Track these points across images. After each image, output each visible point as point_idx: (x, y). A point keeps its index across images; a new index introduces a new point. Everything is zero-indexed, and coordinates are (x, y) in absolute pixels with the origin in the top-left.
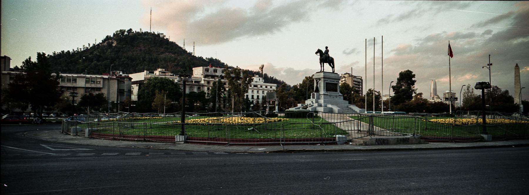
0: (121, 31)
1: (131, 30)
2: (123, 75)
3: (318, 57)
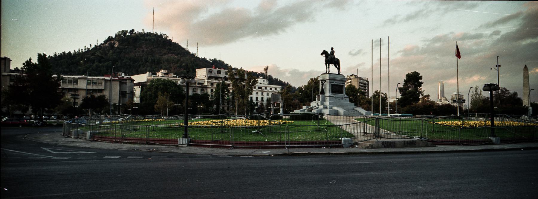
0: (123, 31)
1: (133, 30)
2: (125, 77)
3: (323, 58)
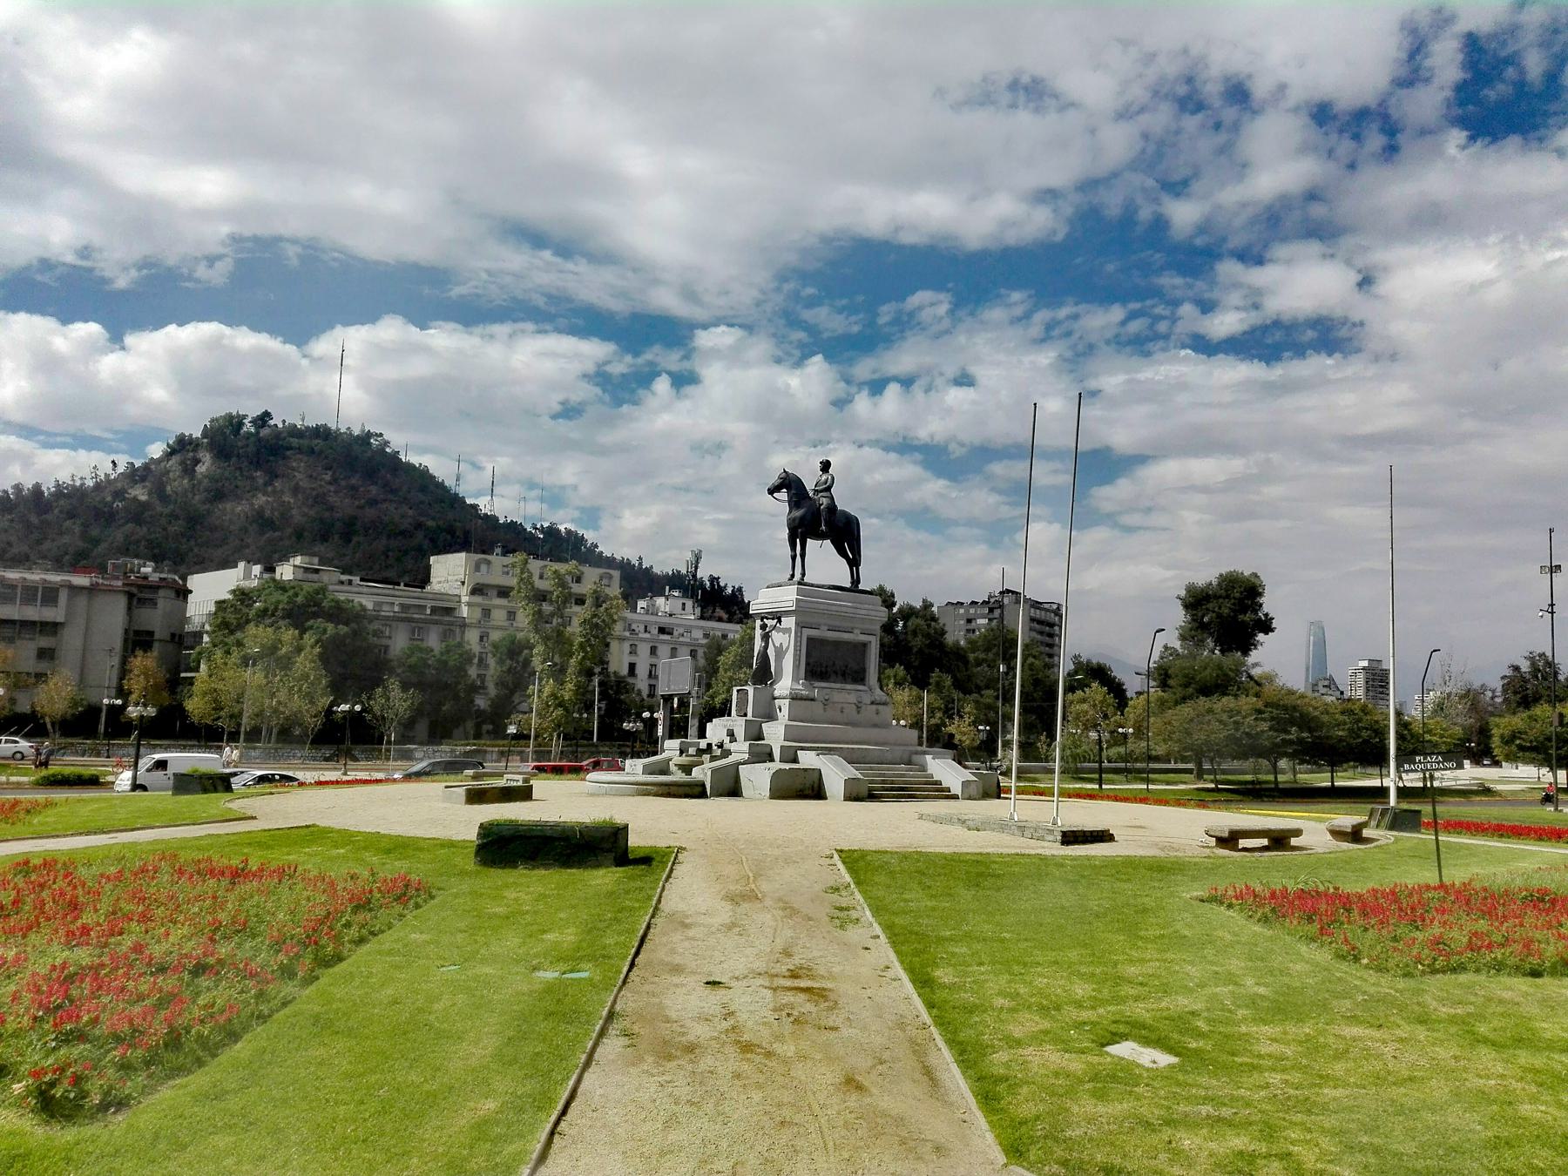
0: (230, 417)
1: (266, 415)
2: (155, 577)
3: (780, 506)
